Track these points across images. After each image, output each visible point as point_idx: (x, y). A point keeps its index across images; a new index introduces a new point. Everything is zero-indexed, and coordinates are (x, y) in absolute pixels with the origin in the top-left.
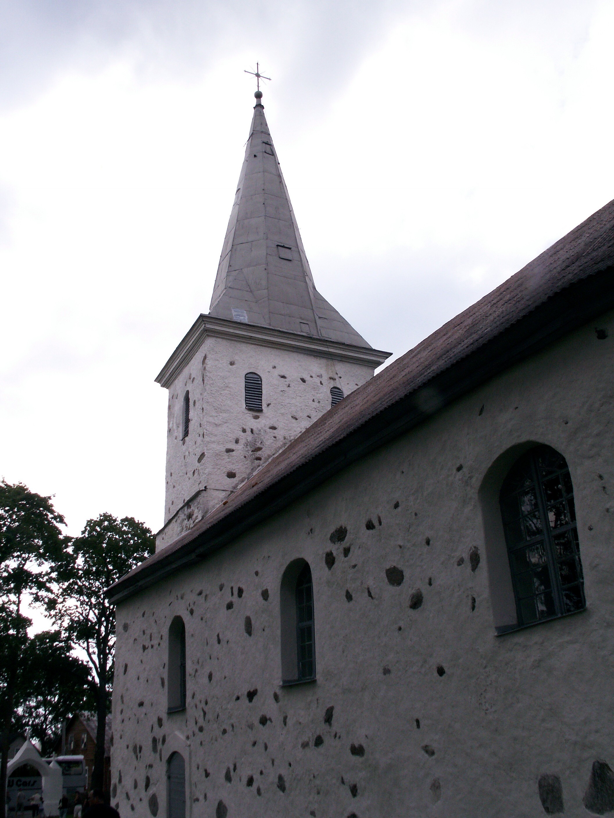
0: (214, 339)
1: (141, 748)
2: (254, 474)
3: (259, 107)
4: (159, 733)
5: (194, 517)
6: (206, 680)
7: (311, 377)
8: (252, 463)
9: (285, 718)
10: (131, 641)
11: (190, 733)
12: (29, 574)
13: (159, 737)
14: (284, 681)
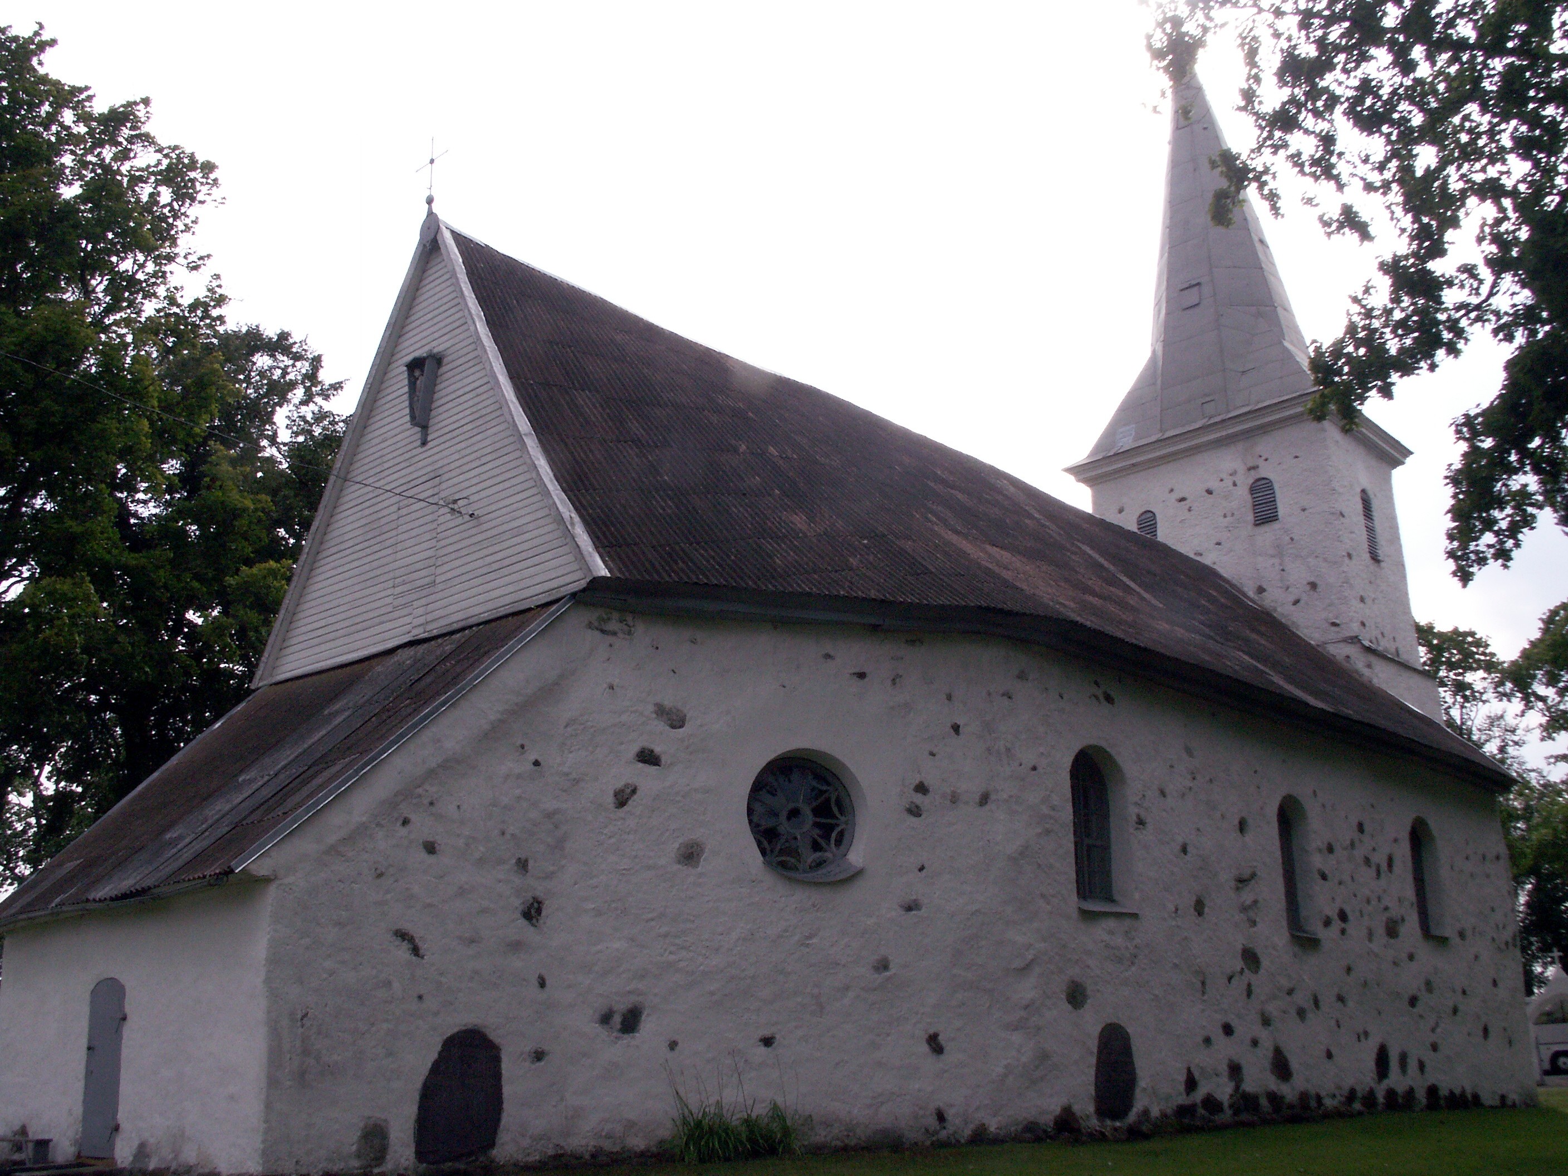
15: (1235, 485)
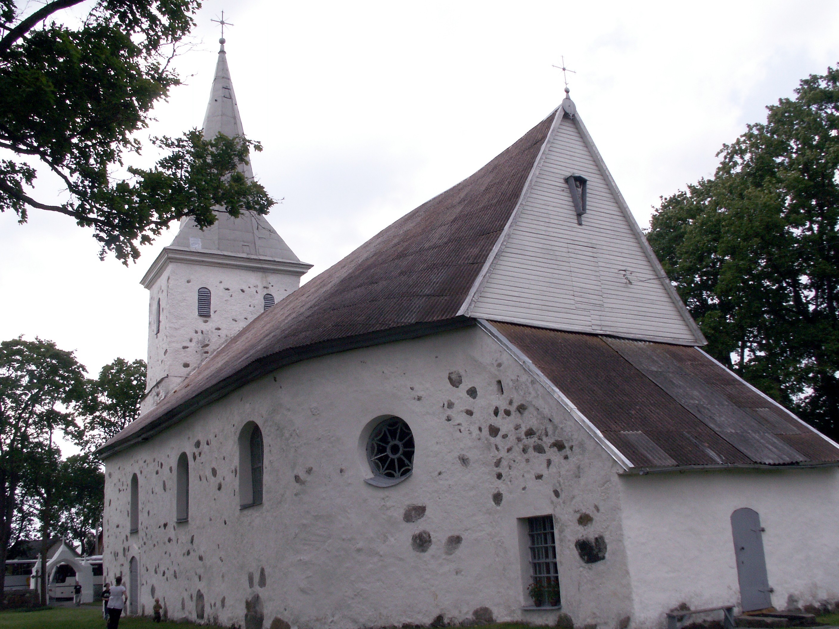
0: (175, 264)
1: (118, 553)
2: (203, 364)
3: (222, 52)
4: (126, 545)
5: (160, 395)
6: (147, 514)
7: (249, 287)
8: (202, 356)
9: (178, 539)
10: (113, 485)
11: (140, 546)
12: (58, 414)
13: (127, 548)
14: (178, 520)
15: (257, 292)
